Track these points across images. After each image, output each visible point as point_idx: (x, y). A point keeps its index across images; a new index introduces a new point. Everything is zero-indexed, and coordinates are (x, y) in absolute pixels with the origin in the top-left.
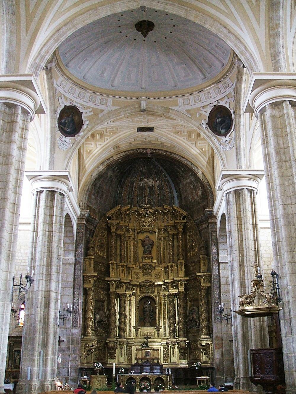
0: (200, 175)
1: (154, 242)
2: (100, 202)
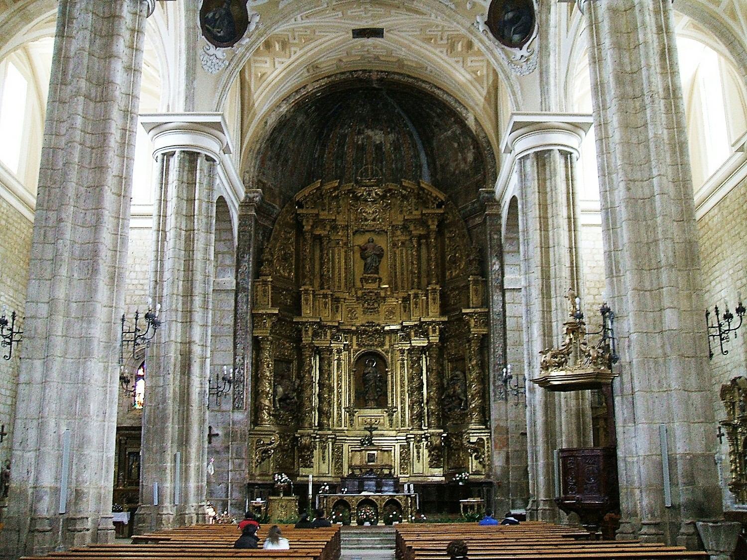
0: (471, 122)
1: (383, 251)
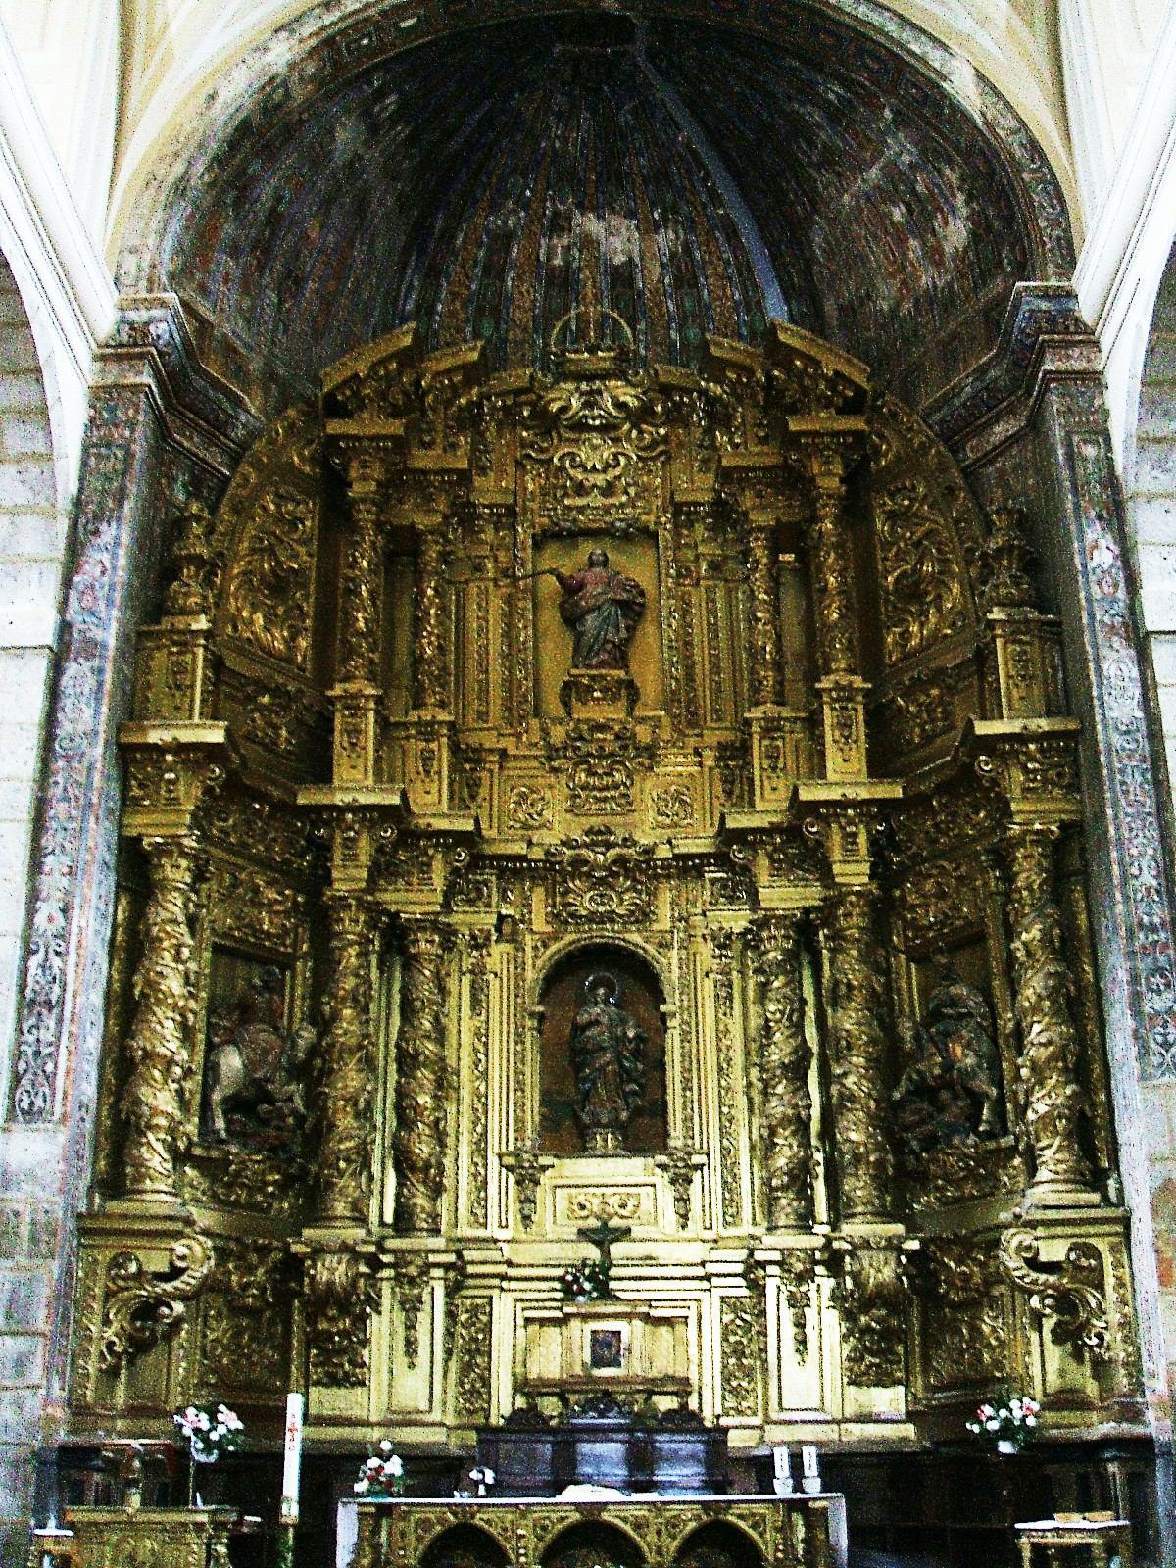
0: (963, 87)
1: (642, 594)
2: (283, 320)
